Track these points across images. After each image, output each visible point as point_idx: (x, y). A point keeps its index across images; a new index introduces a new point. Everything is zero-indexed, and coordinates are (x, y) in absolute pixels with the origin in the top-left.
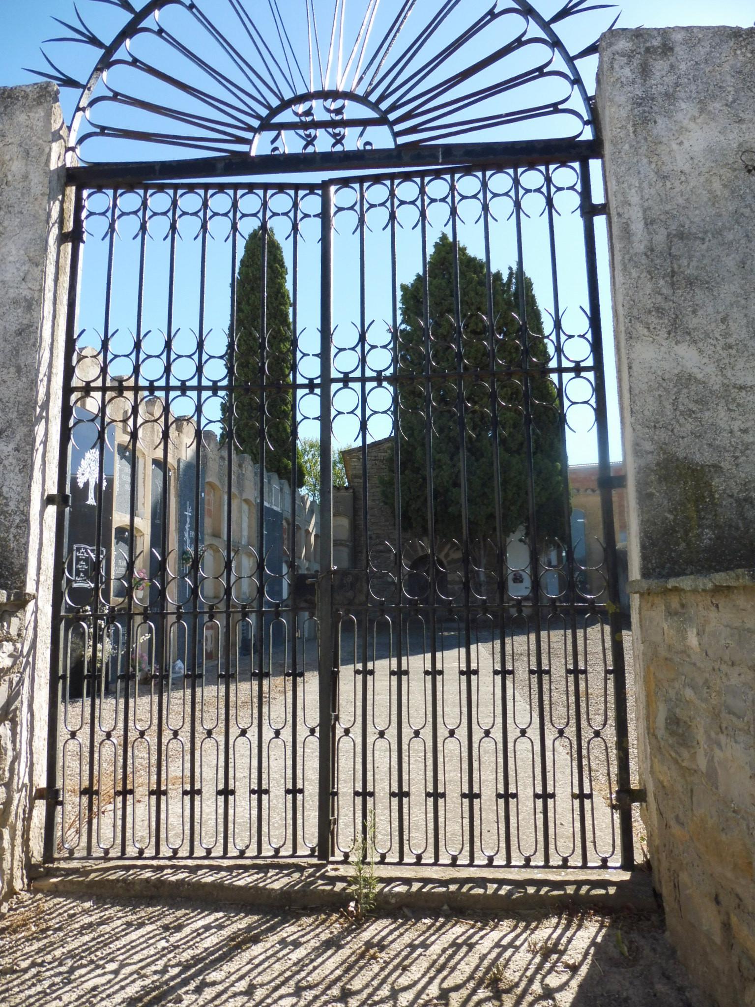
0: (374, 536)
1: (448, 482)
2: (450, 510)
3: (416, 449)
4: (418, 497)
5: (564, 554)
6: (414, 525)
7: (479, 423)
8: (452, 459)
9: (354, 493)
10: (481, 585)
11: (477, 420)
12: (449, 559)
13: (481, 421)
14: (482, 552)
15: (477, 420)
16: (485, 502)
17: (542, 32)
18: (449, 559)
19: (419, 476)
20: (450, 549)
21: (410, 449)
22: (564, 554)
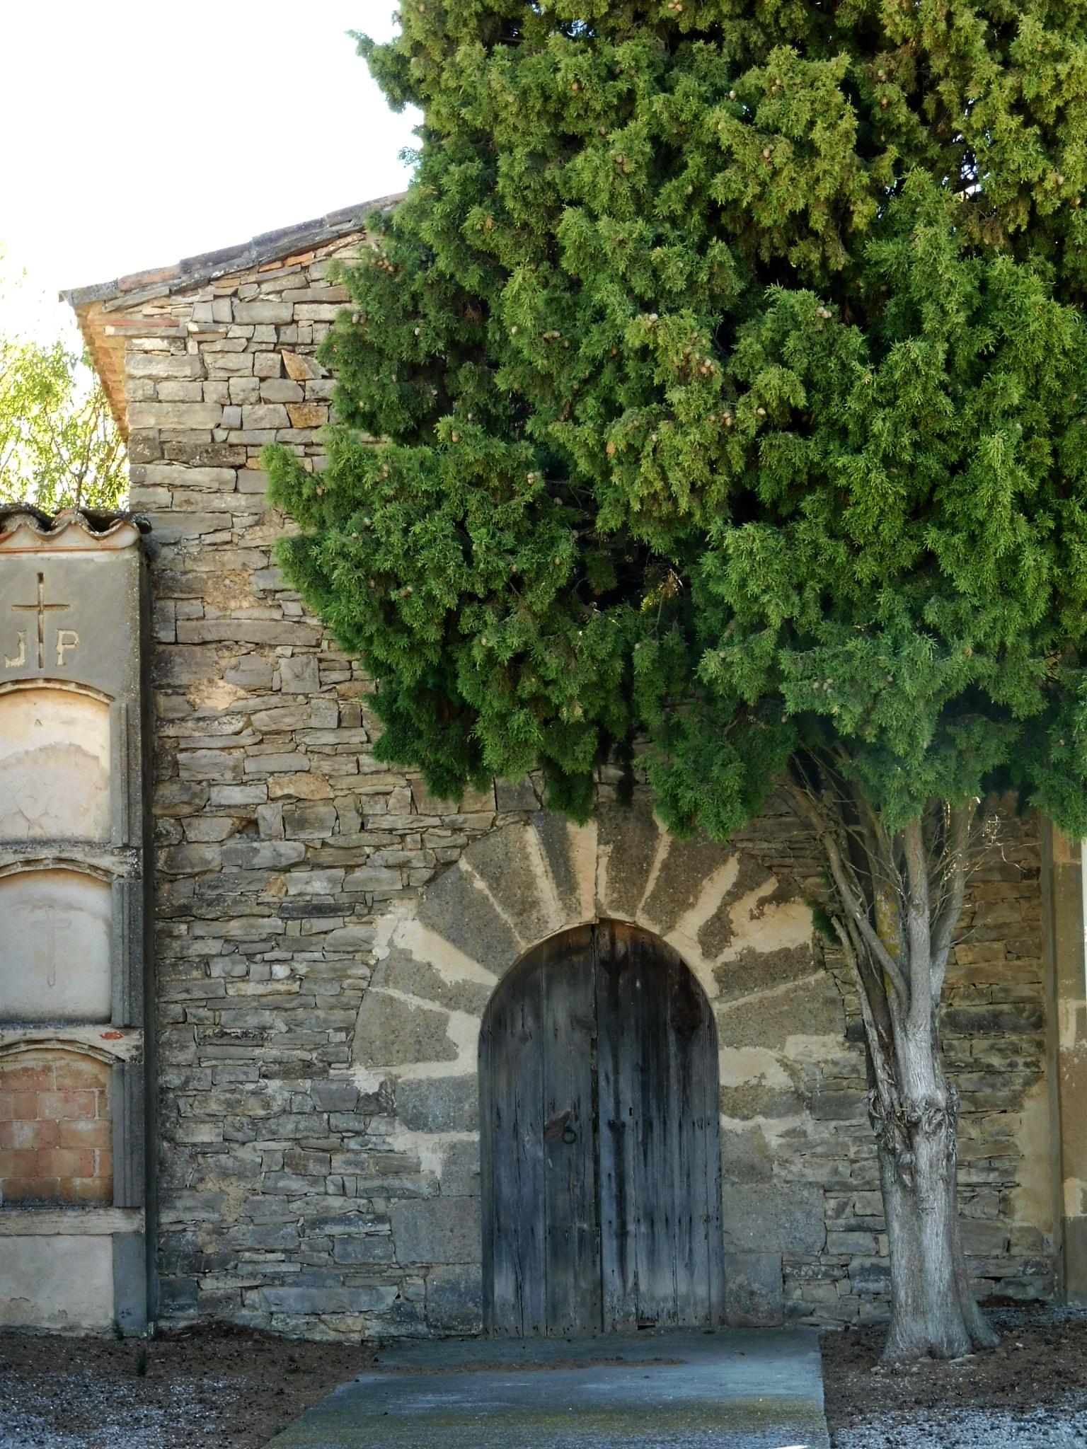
0: (270, 816)
1: (697, 490)
2: (711, 663)
3: (506, 274)
4: (517, 583)
5: (638, 984)
6: (491, 757)
7: (903, 114)
8: (724, 343)
9: (147, 550)
10: (912, 1127)
11: (890, 93)
12: (729, 955)
13: (914, 102)
14: (920, 926)
15: (890, 93)
16: (931, 615)
17: (477, 967)
18: (729, 955)
19: (526, 451)
20: (734, 896)
21: (471, 280)
22: (638, 984)
